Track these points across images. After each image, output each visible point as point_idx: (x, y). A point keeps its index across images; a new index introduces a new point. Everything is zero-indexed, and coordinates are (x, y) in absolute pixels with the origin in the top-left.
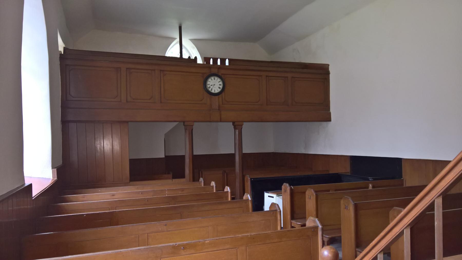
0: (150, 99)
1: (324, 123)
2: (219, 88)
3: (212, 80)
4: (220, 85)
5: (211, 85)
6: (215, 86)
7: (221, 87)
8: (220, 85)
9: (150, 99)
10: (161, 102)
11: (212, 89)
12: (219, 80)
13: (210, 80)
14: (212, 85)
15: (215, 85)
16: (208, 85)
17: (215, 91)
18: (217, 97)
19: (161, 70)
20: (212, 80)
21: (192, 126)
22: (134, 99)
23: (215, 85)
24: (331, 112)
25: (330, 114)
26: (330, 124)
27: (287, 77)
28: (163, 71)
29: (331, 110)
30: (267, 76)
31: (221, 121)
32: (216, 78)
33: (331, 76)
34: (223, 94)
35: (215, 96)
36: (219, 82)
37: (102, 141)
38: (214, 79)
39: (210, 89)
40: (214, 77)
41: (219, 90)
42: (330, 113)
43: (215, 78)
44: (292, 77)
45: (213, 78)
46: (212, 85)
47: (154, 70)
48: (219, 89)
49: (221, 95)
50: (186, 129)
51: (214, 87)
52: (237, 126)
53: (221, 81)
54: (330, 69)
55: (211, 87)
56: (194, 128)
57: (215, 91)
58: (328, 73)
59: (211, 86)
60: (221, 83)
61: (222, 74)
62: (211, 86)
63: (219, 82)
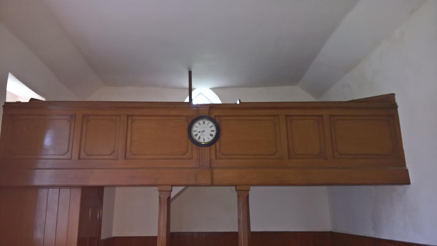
0: (110, 155)
1: (399, 188)
2: (211, 135)
3: (200, 125)
4: (212, 131)
5: (198, 131)
6: (204, 133)
7: (214, 133)
8: (212, 131)
9: (110, 155)
10: (125, 158)
11: (199, 137)
12: (211, 124)
13: (197, 124)
14: (199, 132)
15: (204, 131)
16: (194, 131)
17: (204, 140)
18: (207, 149)
19: (128, 116)
20: (200, 125)
21: (248, 191)
22: (88, 155)
23: (204, 131)
24: (408, 168)
25: (406, 172)
26: (410, 189)
27: (321, 116)
28: (132, 116)
29: (409, 165)
30: (287, 116)
31: (212, 185)
32: (207, 122)
33: (399, 110)
34: (218, 144)
35: (207, 147)
36: (210, 127)
37: (98, 210)
38: (204, 123)
39: (197, 138)
40: (203, 120)
41: (211, 138)
42: (407, 171)
43: (204, 122)
44: (330, 116)
45: (201, 122)
46: (199, 132)
47: (120, 116)
48: (195, 134)
49: (214, 146)
50: (239, 196)
51: (203, 134)
52: (60, 189)
53: (214, 126)
54: (398, 100)
55: (199, 134)
56: (251, 193)
57: (204, 140)
58: (395, 107)
59: (199, 134)
60: (214, 128)
61: (215, 116)
62: (199, 134)
63: (210, 127)
